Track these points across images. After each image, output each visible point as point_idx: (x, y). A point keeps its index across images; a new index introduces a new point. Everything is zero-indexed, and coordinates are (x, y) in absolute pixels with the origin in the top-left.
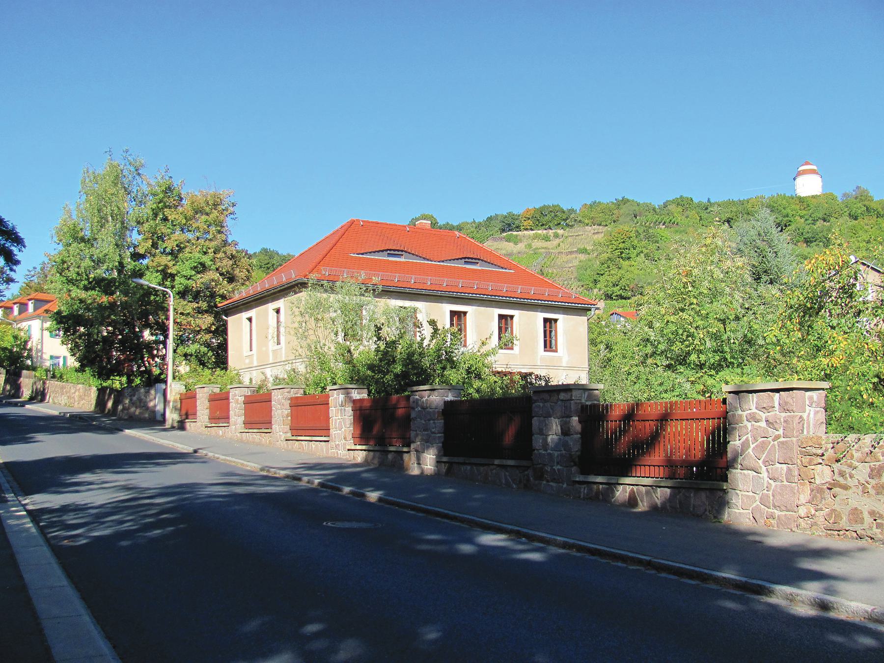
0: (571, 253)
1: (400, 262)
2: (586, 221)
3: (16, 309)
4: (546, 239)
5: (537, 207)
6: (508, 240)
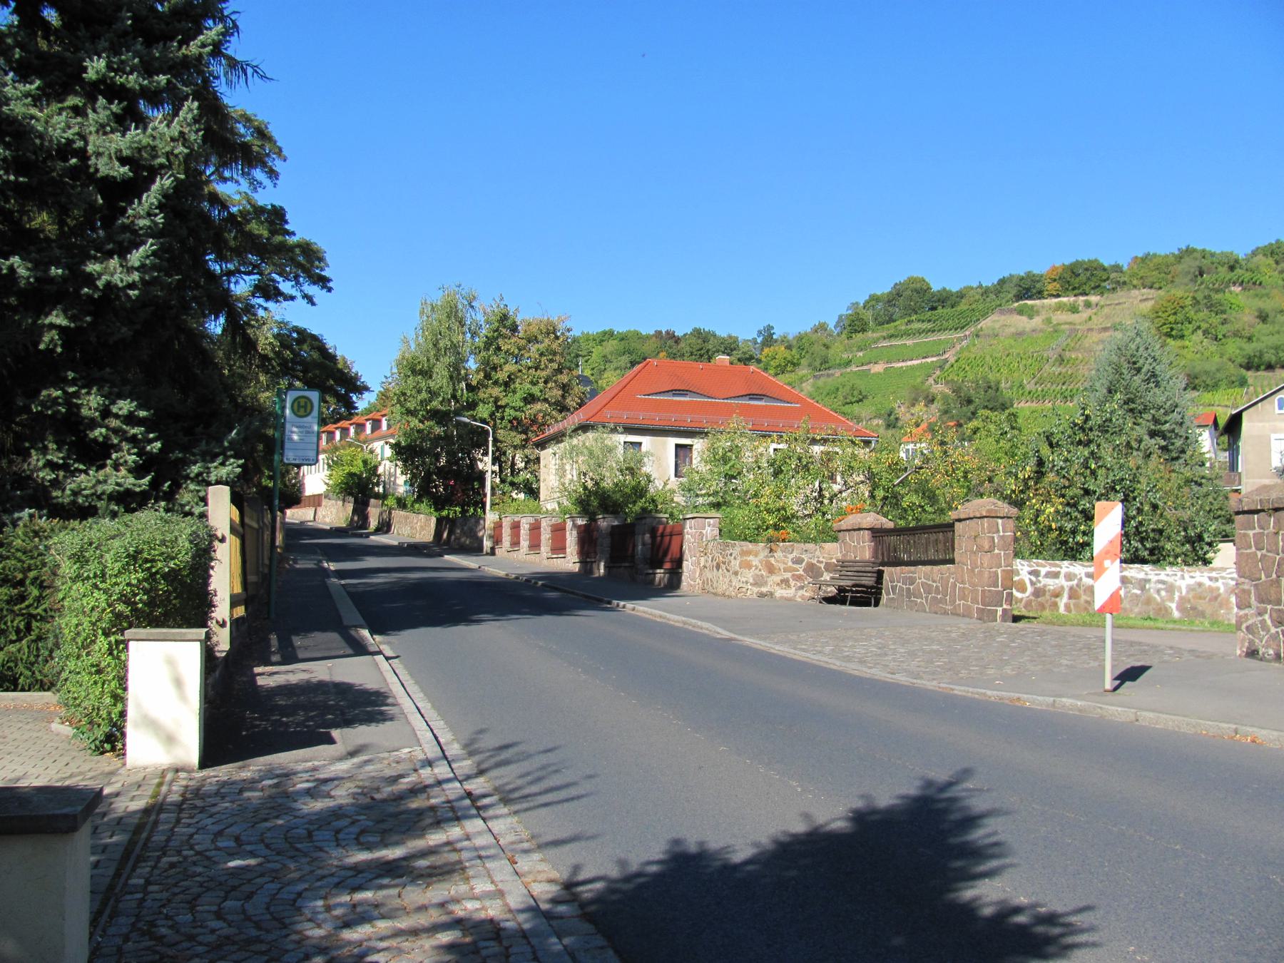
0: (1105, 329)
1: (684, 402)
2: (1135, 282)
3: (369, 426)
4: (1074, 309)
5: (1066, 263)
6: (1020, 312)
